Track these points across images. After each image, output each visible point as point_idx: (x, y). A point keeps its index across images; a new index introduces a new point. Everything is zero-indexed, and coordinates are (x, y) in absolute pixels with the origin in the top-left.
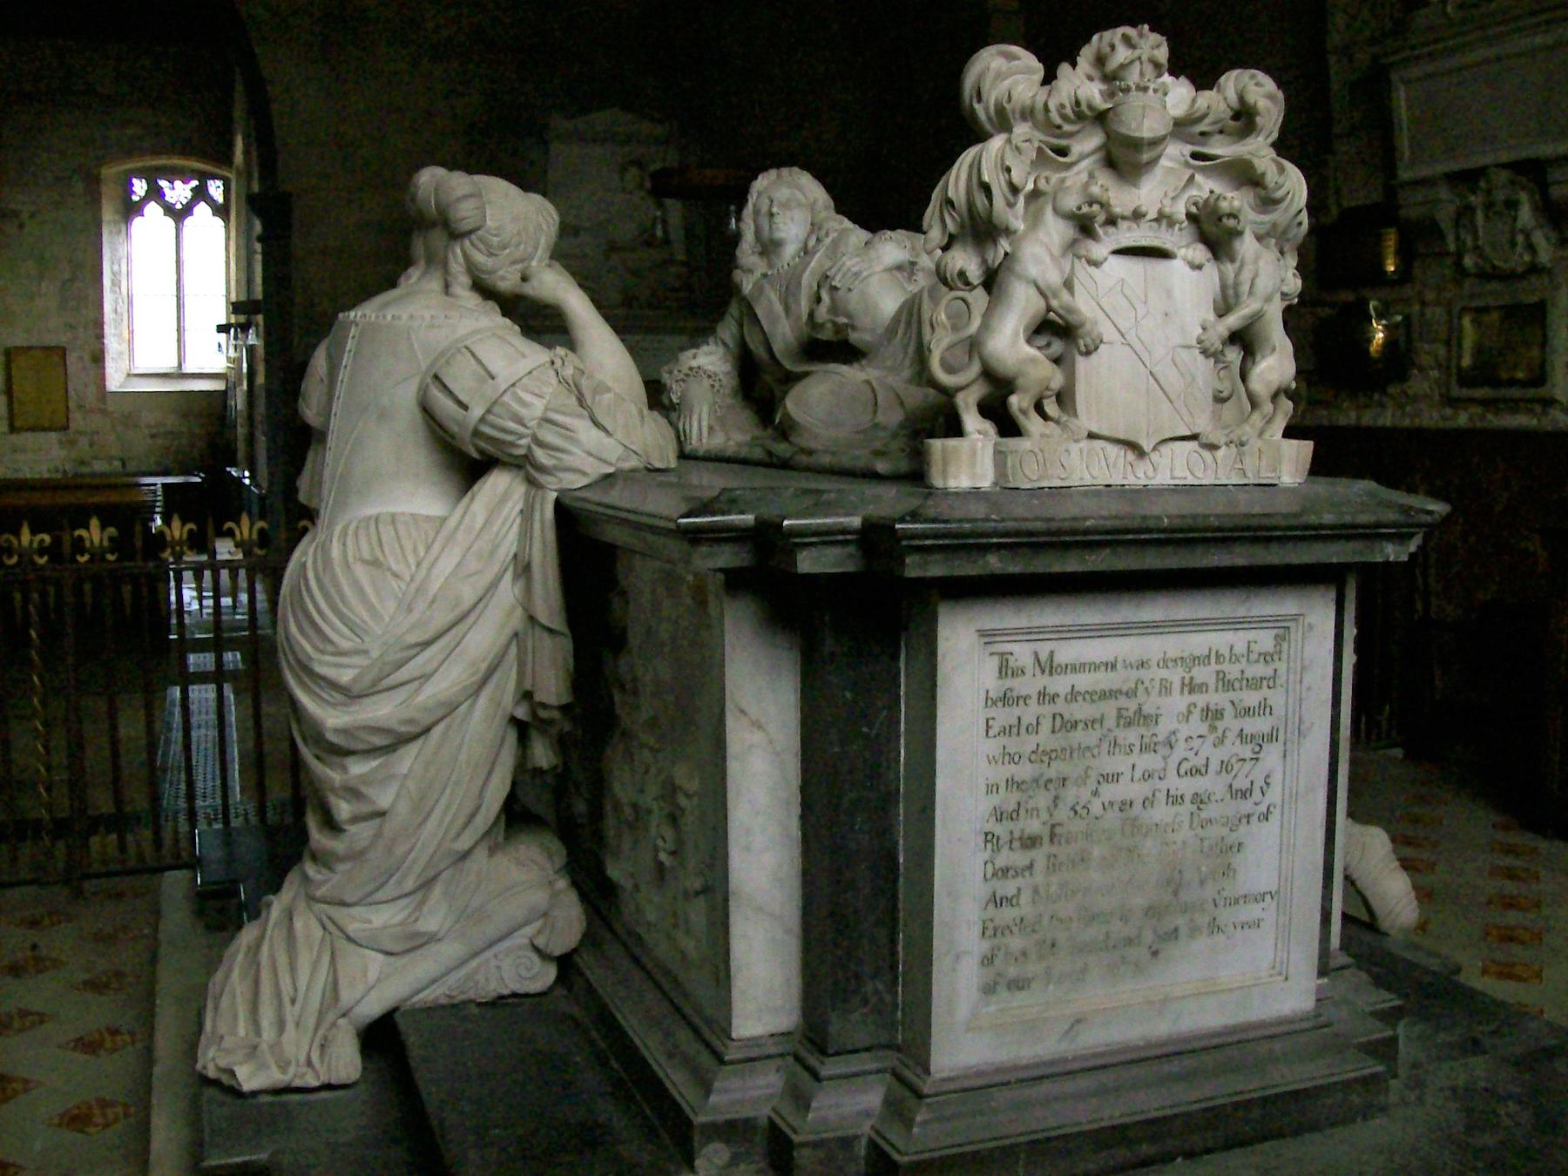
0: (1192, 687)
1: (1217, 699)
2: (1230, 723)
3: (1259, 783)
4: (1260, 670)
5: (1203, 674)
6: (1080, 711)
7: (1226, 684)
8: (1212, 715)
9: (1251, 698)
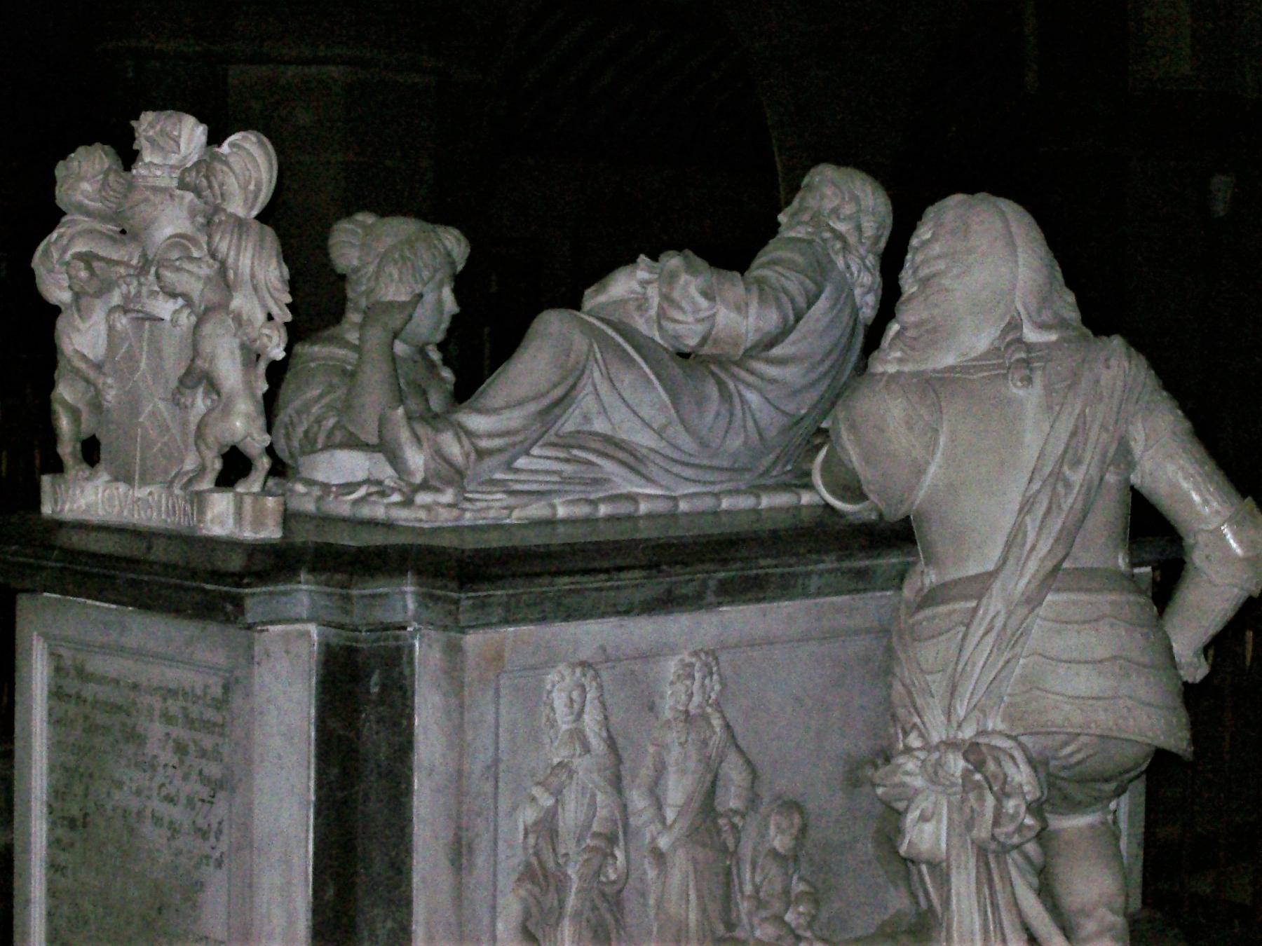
0: (168, 719)
1: (179, 732)
2: (192, 759)
3: (215, 826)
4: (210, 714)
5: (174, 707)
6: (101, 718)
7: (190, 723)
8: (181, 749)
9: (208, 742)
